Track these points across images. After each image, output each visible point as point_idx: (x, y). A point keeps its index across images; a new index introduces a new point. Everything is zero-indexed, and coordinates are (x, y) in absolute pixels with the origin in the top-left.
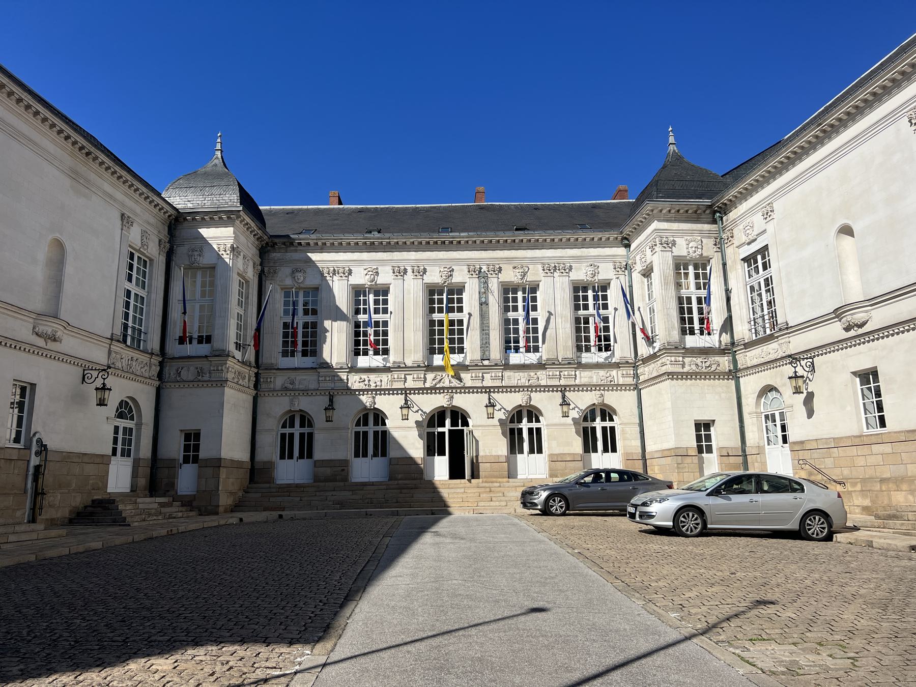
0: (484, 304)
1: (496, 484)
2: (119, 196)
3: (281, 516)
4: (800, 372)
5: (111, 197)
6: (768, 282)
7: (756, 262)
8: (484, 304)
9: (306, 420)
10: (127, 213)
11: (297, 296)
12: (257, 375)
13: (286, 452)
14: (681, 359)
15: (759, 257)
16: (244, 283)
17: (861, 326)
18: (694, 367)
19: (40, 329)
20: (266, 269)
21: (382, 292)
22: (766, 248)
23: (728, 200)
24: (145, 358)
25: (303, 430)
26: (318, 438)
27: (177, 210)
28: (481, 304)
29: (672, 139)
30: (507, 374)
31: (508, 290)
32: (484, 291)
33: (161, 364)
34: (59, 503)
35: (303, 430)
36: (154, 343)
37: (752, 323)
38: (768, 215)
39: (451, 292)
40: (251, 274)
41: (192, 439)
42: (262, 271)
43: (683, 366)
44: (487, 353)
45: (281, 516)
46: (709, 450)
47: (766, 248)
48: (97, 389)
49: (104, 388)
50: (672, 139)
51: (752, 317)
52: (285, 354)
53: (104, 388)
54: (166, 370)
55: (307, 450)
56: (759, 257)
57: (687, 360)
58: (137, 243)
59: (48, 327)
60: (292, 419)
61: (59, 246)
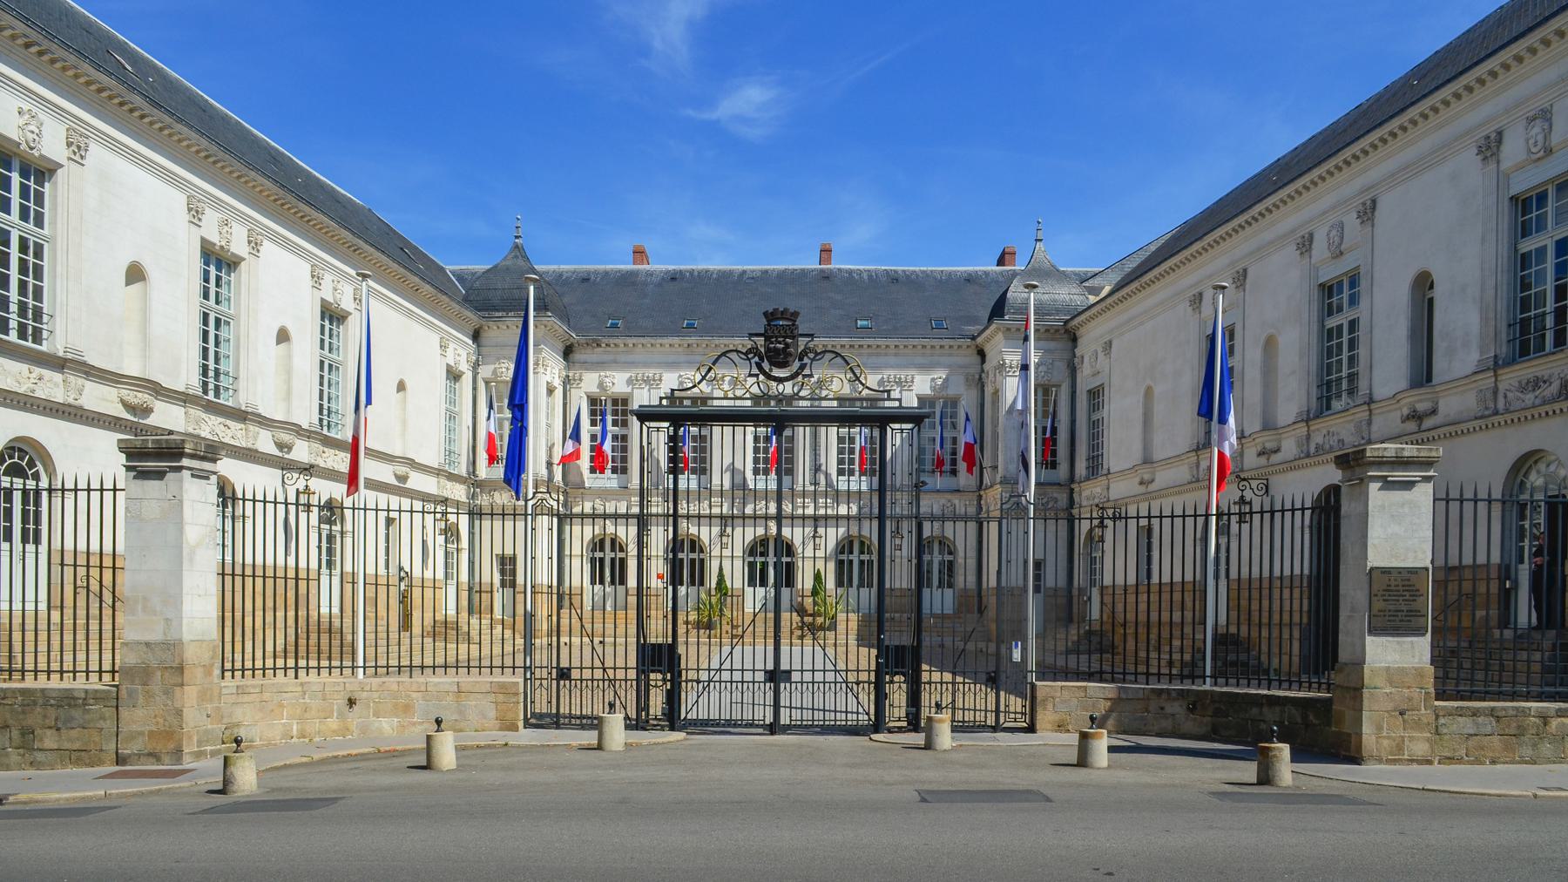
4: (1248, 495)
6: (1353, 325)
35: (692, 556)
41: (507, 565)
45: (778, 344)
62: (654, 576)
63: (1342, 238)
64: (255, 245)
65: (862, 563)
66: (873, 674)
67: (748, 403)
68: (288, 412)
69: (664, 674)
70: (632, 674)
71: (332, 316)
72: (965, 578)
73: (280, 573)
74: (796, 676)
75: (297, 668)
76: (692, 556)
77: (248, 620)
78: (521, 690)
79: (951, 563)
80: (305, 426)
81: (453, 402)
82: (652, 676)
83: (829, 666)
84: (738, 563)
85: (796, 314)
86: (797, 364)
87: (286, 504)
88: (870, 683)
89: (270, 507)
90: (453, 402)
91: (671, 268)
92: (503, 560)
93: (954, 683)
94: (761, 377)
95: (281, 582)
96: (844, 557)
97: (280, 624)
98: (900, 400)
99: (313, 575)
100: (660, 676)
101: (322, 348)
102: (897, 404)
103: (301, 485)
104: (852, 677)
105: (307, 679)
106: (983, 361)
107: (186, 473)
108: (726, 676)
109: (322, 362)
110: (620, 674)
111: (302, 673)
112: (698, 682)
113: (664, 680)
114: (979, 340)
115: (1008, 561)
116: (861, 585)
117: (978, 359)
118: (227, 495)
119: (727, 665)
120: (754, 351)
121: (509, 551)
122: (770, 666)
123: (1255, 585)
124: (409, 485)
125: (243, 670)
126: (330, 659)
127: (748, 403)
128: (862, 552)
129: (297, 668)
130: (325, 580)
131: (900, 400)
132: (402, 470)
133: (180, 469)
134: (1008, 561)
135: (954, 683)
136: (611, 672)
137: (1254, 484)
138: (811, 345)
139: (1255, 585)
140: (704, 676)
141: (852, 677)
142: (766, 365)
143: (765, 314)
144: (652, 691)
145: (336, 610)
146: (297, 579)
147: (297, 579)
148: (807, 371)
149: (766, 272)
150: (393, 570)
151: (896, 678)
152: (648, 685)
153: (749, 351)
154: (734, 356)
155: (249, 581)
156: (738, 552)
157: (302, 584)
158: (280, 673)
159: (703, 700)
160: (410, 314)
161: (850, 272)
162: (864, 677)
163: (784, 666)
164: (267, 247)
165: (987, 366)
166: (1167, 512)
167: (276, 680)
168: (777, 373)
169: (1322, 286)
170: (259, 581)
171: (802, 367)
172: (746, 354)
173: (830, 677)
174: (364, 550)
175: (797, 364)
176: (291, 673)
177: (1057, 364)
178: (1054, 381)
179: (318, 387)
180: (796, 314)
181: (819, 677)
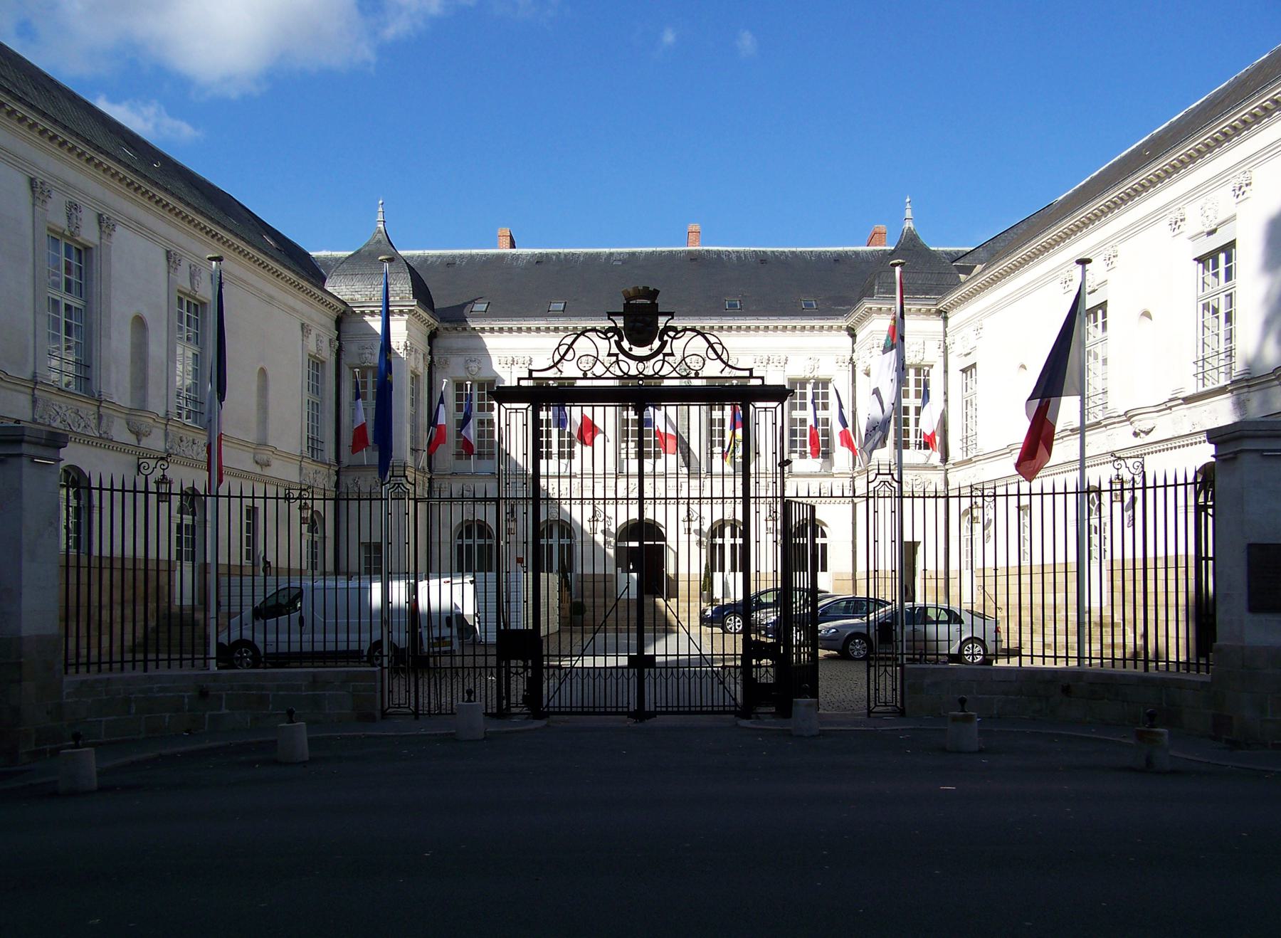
1: (600, 601)
2: (299, 305)
3: (641, 322)
5: (294, 309)
7: (1216, 266)
9: (483, 529)
10: (307, 322)
12: (430, 480)
15: (1222, 257)
16: (415, 377)
17: (1147, 433)
19: (258, 457)
20: (436, 359)
22: (1232, 244)
23: (1271, 100)
24: (324, 470)
25: (482, 542)
27: (344, 303)
29: (908, 214)
33: (338, 473)
36: (329, 454)
37: (1200, 363)
38: (1239, 191)
40: (422, 370)
45: (641, 322)
47: (1232, 244)
50: (908, 214)
51: (1200, 354)
54: (342, 478)
56: (1222, 257)
58: (186, 286)
59: (263, 457)
61: (263, 372)
62: (514, 561)
63: (219, 376)
65: (561, 547)
69: (525, 661)
70: (492, 661)
75: (146, 661)
76: (470, 542)
79: (570, 547)
82: (513, 663)
85: (656, 293)
86: (656, 344)
87: (112, 490)
88: (548, 656)
89: (129, 496)
91: (537, 251)
92: (369, 546)
94: (621, 357)
98: (762, 378)
100: (521, 663)
102: (759, 382)
103: (158, 474)
105: (135, 674)
107: (25, 461)
111: (151, 665)
113: (525, 668)
118: (77, 480)
121: (376, 539)
123: (129, 565)
124: (268, 472)
125: (111, 662)
126: (158, 653)
129: (146, 661)
131: (762, 378)
133: (20, 455)
137: (1130, 462)
138: (670, 324)
139: (129, 565)
142: (626, 344)
144: (513, 679)
148: (667, 350)
149: (634, 254)
151: (764, 662)
152: (508, 673)
158: (128, 666)
159: (566, 688)
161: (719, 253)
166: (1059, 489)
167: (126, 674)
168: (637, 351)
171: (664, 344)
175: (656, 344)
176: (140, 665)
178: (928, 360)
180: (656, 293)
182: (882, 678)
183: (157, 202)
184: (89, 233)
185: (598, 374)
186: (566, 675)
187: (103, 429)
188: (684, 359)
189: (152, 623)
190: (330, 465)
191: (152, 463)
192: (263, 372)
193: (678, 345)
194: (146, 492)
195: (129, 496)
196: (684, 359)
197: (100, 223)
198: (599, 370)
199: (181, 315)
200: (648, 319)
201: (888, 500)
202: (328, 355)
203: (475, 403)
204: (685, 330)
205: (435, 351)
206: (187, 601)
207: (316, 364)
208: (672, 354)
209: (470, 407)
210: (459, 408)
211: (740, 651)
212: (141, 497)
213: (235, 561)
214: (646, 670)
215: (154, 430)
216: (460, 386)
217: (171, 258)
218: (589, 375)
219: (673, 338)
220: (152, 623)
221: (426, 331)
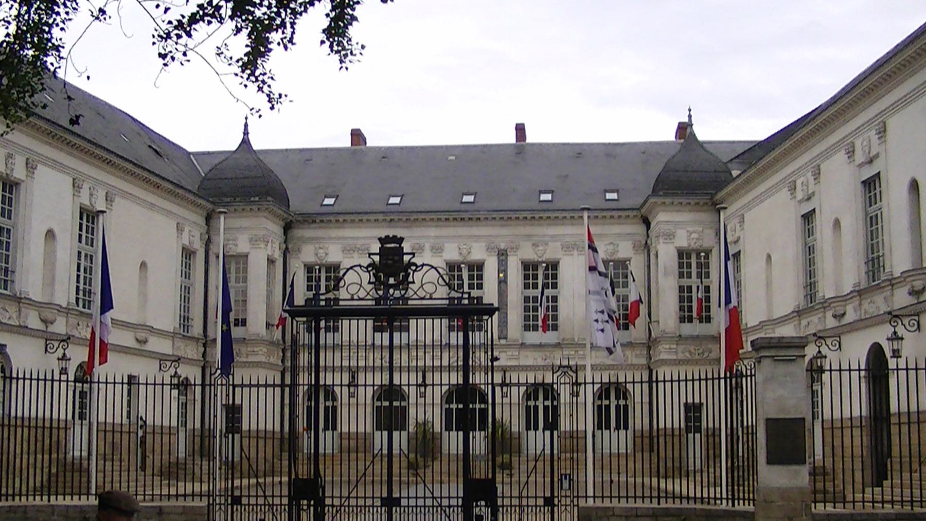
0: (503, 282)
8: (503, 282)
11: (320, 272)
13: (531, 424)
14: (675, 346)
18: (688, 354)
20: (290, 246)
21: (553, 266)
26: (343, 413)
28: (500, 282)
30: (524, 353)
31: (529, 268)
32: (502, 267)
34: (155, 460)
39: (471, 267)
42: (287, 248)
43: (676, 353)
44: (505, 332)
46: (698, 430)
48: (59, 359)
49: (64, 358)
52: (527, 328)
53: (64, 358)
55: (552, 425)
57: (681, 348)
58: (87, 203)
60: (608, 392)
64: (30, 167)
66: (460, 501)
67: (370, 303)
68: (52, 295)
69: (309, 501)
70: (285, 501)
71: (89, 217)
72: (639, 419)
73: (40, 424)
74: (404, 502)
77: (18, 461)
78: (206, 512)
80: (64, 305)
81: (187, 276)
83: (428, 494)
84: (437, 411)
90: (187, 276)
93: (520, 506)
95: (40, 431)
96: (531, 403)
97: (39, 465)
99: (70, 425)
101: (80, 241)
104: (445, 502)
106: (648, 227)
108: (353, 502)
109: (79, 253)
110: (277, 501)
112: (333, 506)
114: (643, 211)
115: (571, 415)
116: (618, 428)
117: (642, 229)
119: (354, 494)
120: (372, 265)
122: (385, 495)
127: (370, 303)
128: (546, 398)
130: (78, 428)
132: (142, 335)
134: (571, 415)
135: (520, 506)
136: (270, 499)
140: (337, 502)
141: (445, 502)
143: (380, 239)
145: (85, 454)
146: (51, 428)
147: (51, 428)
150: (133, 419)
153: (369, 265)
154: (358, 269)
155: (19, 430)
156: (438, 400)
157: (55, 431)
160: (152, 206)
162: (453, 502)
163: (396, 495)
164: (41, 170)
165: (652, 233)
169: (863, 182)
170: (26, 430)
172: (367, 268)
173: (429, 502)
174: (108, 406)
177: (707, 231)
179: (75, 273)
180: (402, 239)
181: (420, 502)
182: (564, 514)
183: (68, 143)
184: (19, 173)
185: (361, 296)
186: (337, 512)
187: (22, 320)
188: (422, 286)
189: (54, 470)
190: (198, 339)
191: (56, 344)
192: (143, 265)
193: (418, 276)
194: (53, 380)
195: (41, 383)
196: (422, 286)
197: (27, 164)
198: (362, 294)
199: (80, 236)
200: (396, 258)
201: (567, 386)
202: (198, 246)
203: (323, 283)
204: (423, 265)
205: (288, 240)
206: (182, 455)
207: (188, 254)
208: (413, 282)
209: (318, 287)
210: (309, 288)
211: (461, 494)
212: (49, 383)
213: (118, 420)
214: (394, 509)
215: (59, 318)
216: (309, 269)
217: (76, 186)
218: (355, 297)
219: (414, 271)
220: (54, 470)
221: (282, 223)
